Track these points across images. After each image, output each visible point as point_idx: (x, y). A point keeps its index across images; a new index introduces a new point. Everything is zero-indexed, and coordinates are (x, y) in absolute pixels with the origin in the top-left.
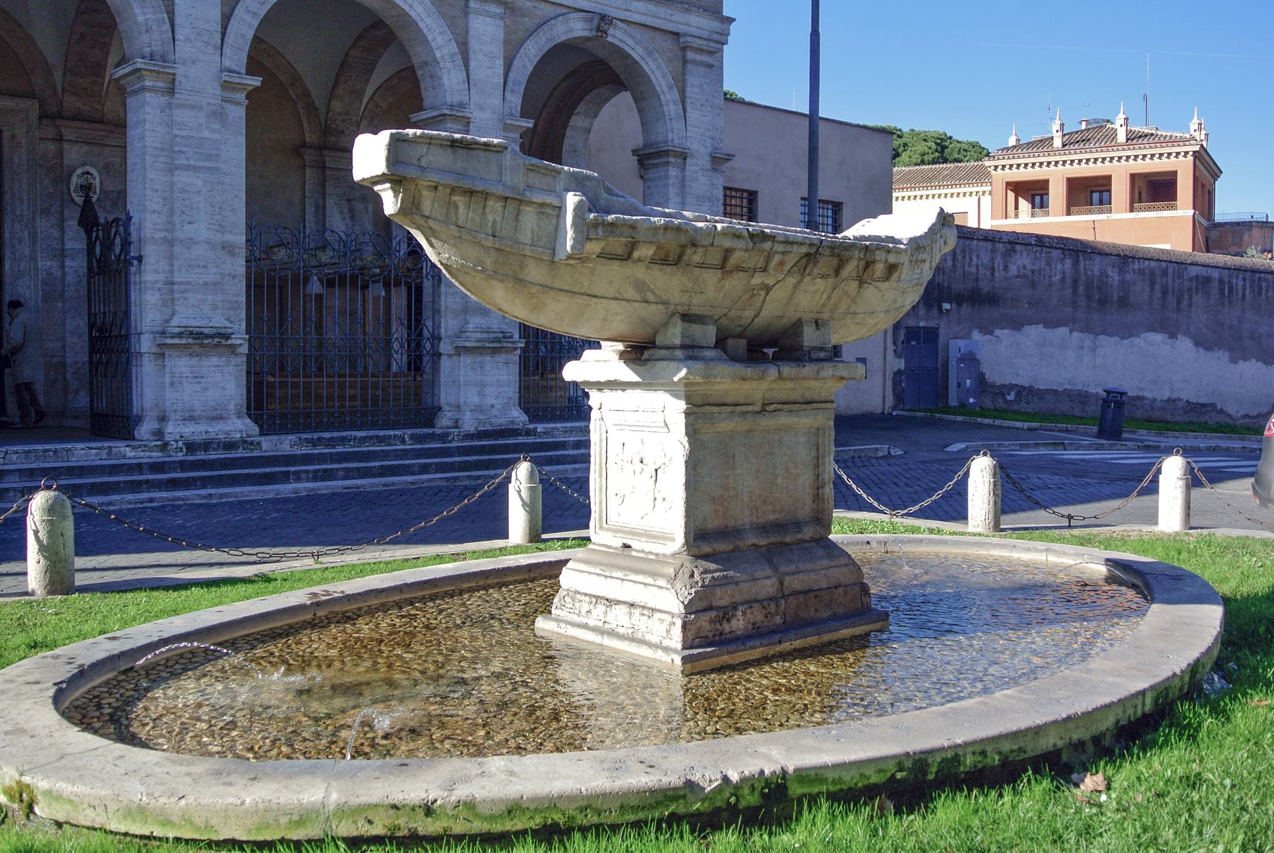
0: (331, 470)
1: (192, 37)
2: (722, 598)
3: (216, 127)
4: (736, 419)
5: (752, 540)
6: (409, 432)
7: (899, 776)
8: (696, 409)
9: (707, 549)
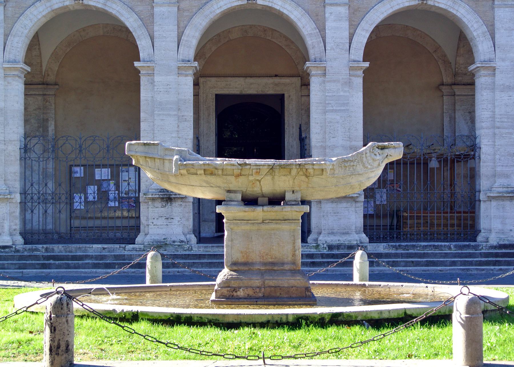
0: (397, 261)
1: (334, 47)
2: (234, 284)
3: (347, 89)
4: (249, 225)
5: (257, 267)
6: (454, 243)
7: (171, 318)
8: (230, 221)
9: (235, 268)
